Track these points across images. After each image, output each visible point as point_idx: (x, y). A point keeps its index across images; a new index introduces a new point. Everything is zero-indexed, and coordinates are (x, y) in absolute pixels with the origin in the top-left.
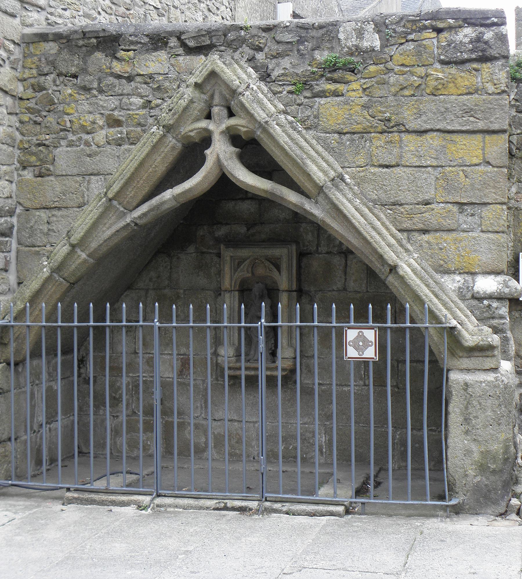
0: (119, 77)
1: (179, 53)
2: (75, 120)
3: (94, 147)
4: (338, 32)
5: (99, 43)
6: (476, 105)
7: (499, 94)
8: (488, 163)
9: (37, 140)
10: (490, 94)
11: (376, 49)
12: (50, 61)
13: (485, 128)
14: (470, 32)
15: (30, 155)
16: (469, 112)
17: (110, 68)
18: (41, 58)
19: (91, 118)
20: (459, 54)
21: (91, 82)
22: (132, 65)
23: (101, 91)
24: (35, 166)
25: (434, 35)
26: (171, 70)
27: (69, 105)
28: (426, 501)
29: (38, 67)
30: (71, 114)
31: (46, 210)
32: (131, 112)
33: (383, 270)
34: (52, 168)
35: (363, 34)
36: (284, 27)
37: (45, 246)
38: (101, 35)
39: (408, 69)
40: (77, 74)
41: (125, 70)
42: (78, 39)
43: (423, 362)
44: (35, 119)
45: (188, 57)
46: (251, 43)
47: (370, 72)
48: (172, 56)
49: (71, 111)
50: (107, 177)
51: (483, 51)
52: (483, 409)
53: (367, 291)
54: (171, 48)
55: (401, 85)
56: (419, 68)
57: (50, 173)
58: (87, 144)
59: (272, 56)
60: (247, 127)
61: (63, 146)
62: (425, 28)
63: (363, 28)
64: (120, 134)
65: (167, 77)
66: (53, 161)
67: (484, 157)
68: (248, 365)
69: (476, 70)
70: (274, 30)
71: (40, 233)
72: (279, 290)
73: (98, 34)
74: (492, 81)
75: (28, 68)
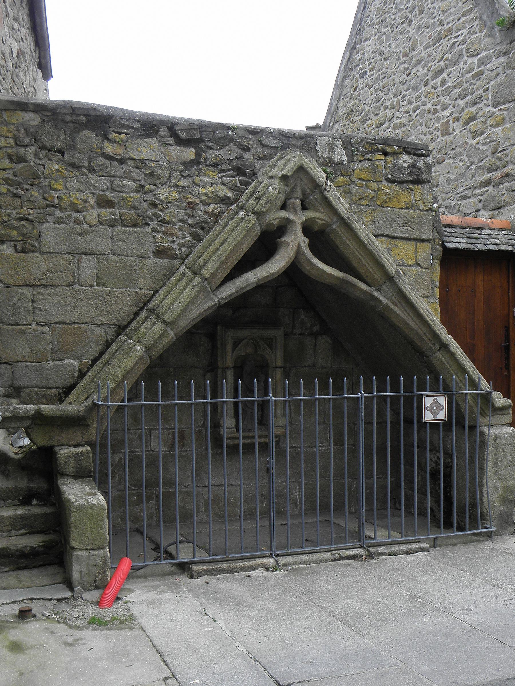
0: (110, 158)
1: (170, 143)
2: (65, 197)
3: (85, 226)
4: (316, 144)
5: (88, 122)
6: (412, 218)
7: (426, 211)
8: (419, 265)
9: (17, 213)
10: (421, 210)
11: (344, 163)
12: (31, 133)
13: (418, 237)
14: (408, 159)
15: (10, 229)
16: (407, 223)
17: (101, 148)
18: (18, 127)
19: (83, 196)
20: (401, 176)
21: (81, 160)
22: (124, 147)
23: (92, 170)
24: (16, 241)
25: (383, 157)
26: (162, 158)
27: (56, 180)
28: (478, 529)
29: (15, 138)
30: (59, 190)
31: (29, 288)
32: (124, 195)
33: (433, 348)
34: (36, 244)
35: (334, 149)
36: (269, 133)
37: (30, 325)
38: (92, 113)
39: (364, 183)
40: (63, 150)
41: (117, 152)
42: (65, 114)
43: (372, 423)
44: (15, 191)
45: (178, 148)
46: (239, 142)
47: (339, 181)
48: (163, 144)
49: (59, 188)
50: (99, 257)
51: (417, 175)
52: (505, 455)
53: (331, 367)
54: (162, 137)
55: (361, 195)
56: (373, 183)
57: (35, 249)
58: (78, 222)
59: (259, 157)
60: (324, 221)
61: (50, 222)
62: (378, 150)
63: (334, 143)
64: (113, 215)
65: (159, 164)
66: (38, 237)
67: (416, 260)
68: (247, 434)
69: (411, 190)
70: (260, 135)
71: (25, 311)
72: (233, 368)
73: (89, 112)
74: (422, 199)
75: (4, 136)
